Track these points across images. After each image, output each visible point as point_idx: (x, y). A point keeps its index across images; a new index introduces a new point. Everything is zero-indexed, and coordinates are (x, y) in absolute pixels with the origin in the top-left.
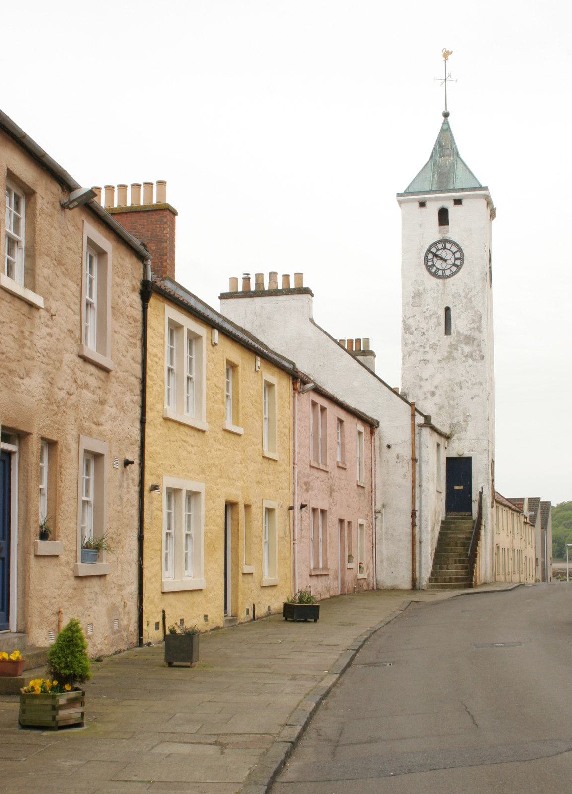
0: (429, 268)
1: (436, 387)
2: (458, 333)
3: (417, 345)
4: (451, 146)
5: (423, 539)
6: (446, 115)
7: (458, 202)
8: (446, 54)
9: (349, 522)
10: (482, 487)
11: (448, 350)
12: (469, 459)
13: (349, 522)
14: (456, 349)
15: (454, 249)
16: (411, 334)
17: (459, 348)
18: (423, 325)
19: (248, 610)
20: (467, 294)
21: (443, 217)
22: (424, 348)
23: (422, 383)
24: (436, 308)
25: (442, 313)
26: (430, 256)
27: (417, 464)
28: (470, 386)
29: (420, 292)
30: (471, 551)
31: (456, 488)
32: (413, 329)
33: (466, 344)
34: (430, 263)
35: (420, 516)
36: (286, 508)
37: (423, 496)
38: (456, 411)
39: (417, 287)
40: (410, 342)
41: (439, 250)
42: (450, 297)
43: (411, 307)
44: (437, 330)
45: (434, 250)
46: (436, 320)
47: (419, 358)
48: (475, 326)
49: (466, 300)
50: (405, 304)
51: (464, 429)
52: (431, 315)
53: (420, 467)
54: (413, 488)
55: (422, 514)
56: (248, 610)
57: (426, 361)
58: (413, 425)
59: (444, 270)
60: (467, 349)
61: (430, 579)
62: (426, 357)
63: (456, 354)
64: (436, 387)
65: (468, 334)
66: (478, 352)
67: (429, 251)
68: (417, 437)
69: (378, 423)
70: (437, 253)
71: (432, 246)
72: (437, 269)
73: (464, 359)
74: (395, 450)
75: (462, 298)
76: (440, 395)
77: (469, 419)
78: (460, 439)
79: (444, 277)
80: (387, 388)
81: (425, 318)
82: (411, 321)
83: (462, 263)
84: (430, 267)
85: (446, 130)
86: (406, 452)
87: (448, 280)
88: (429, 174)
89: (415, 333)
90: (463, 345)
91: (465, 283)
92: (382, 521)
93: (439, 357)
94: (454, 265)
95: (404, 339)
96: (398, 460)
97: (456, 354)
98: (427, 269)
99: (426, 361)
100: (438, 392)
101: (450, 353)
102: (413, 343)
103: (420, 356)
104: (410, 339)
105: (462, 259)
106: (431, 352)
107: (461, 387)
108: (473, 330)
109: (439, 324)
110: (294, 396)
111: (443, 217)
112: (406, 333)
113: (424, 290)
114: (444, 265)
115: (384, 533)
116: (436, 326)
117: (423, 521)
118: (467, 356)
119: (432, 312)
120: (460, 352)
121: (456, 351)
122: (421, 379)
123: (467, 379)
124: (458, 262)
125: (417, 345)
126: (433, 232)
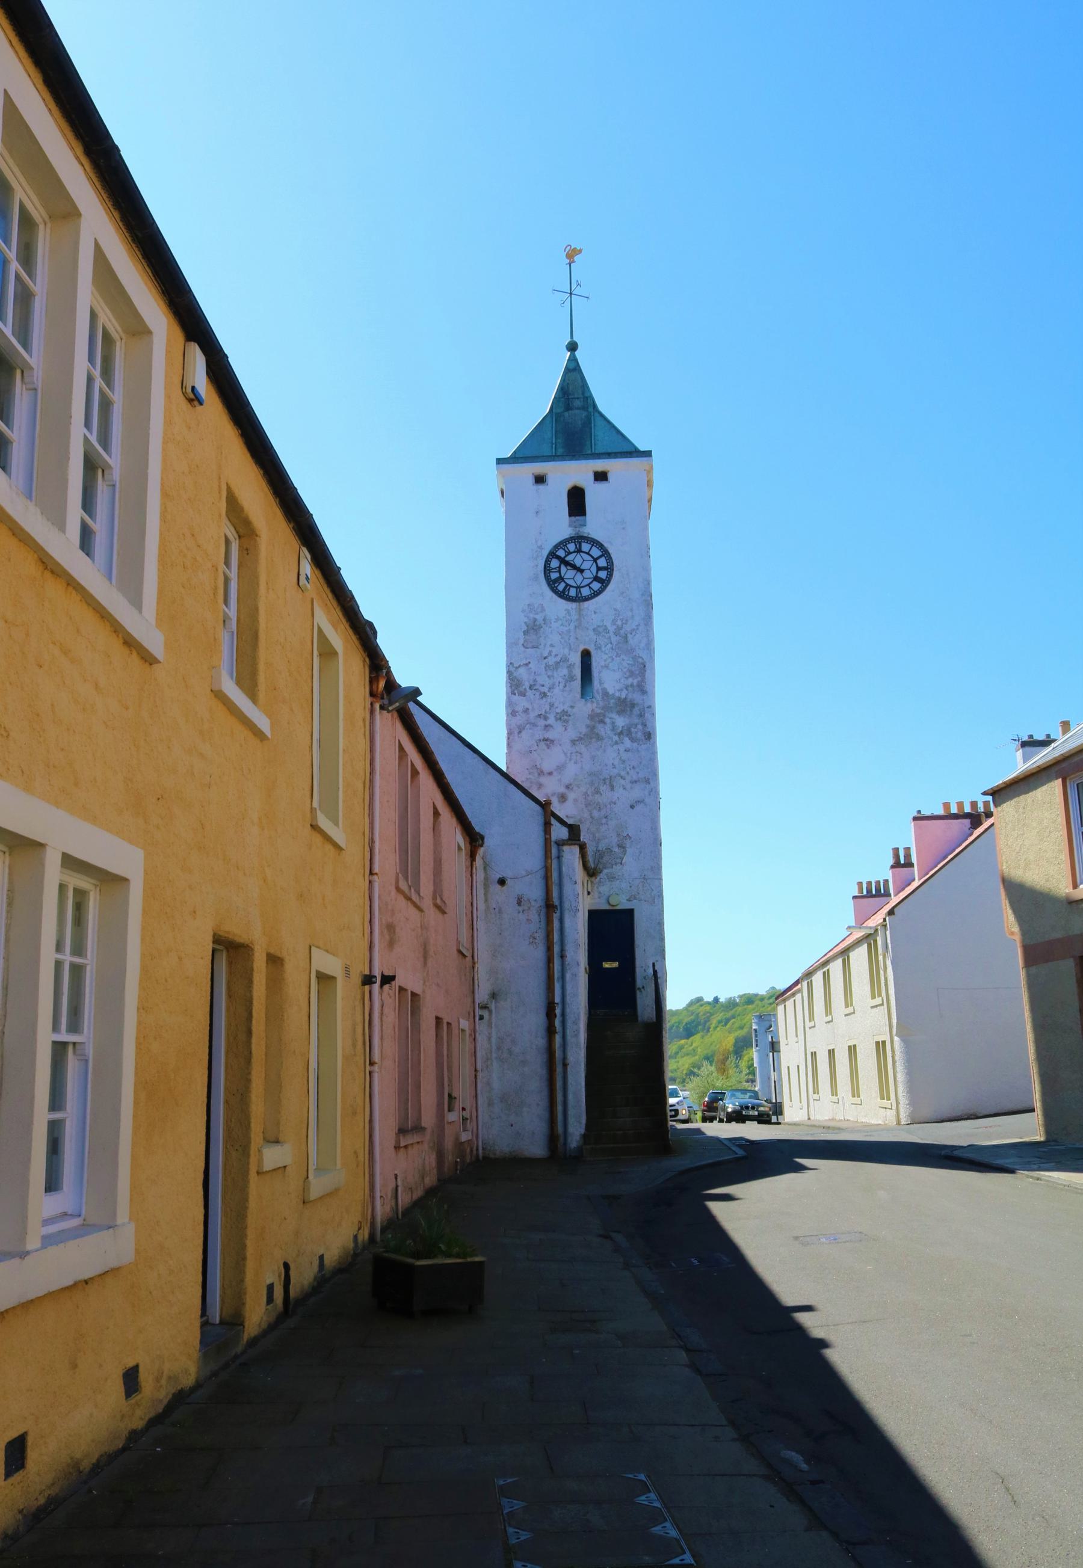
0: (552, 584)
1: (567, 787)
2: (605, 694)
3: (532, 715)
4: (583, 393)
5: (571, 1059)
6: (572, 347)
7: (601, 477)
8: (572, 255)
9: (449, 1024)
10: (654, 965)
11: (588, 722)
12: (630, 913)
13: (449, 1024)
14: (602, 722)
15: (596, 552)
16: (523, 694)
17: (607, 720)
18: (543, 679)
19: (270, 1288)
20: (619, 628)
21: (577, 501)
22: (546, 718)
23: (543, 780)
24: (566, 651)
25: (576, 659)
26: (555, 563)
27: (556, 916)
28: (628, 786)
29: (537, 623)
30: (762, 1083)
31: (606, 965)
32: (527, 685)
33: (621, 712)
34: (554, 576)
35: (563, 1014)
36: (357, 980)
37: (568, 976)
38: (603, 828)
39: (532, 616)
40: (520, 709)
41: (570, 553)
42: (591, 633)
43: (523, 649)
44: (567, 688)
45: (561, 553)
46: (565, 671)
47: (537, 737)
48: (635, 682)
49: (618, 638)
50: (511, 645)
51: (619, 861)
52: (557, 663)
53: (561, 921)
54: (550, 960)
55: (568, 1010)
56: (270, 1288)
57: (549, 742)
58: (547, 842)
59: (578, 588)
60: (621, 722)
61: (585, 1137)
62: (550, 735)
63: (604, 730)
64: (567, 787)
65: (623, 696)
66: (640, 727)
67: (552, 555)
68: (555, 865)
69: (482, 838)
70: (567, 559)
71: (557, 547)
72: (567, 585)
73: (616, 738)
74: (515, 888)
75: (611, 634)
76: (575, 800)
77: (628, 843)
78: (612, 878)
79: (579, 599)
80: (498, 775)
81: (547, 667)
82: (522, 673)
83: (610, 576)
84: (556, 581)
85: (573, 370)
86: (535, 892)
87: (586, 604)
88: (548, 434)
89: (529, 693)
90: (614, 716)
91: (615, 610)
92: (490, 1025)
93: (572, 734)
94: (596, 579)
95: (510, 704)
96: (521, 909)
97: (604, 730)
98: (549, 585)
99: (549, 742)
100: (571, 796)
101: (592, 728)
102: (526, 711)
103: (540, 734)
104: (522, 703)
105: (609, 569)
106: (558, 727)
107: (612, 788)
108: (630, 689)
109: (572, 678)
110: (372, 712)
111: (577, 501)
112: (513, 693)
113: (544, 620)
114: (579, 578)
115: (494, 1047)
116: (567, 681)
117: (569, 1024)
118: (621, 733)
119: (558, 659)
120: (608, 727)
121: (602, 725)
122: (541, 773)
123: (623, 773)
124: (603, 574)
125: (532, 715)
126: (561, 526)
